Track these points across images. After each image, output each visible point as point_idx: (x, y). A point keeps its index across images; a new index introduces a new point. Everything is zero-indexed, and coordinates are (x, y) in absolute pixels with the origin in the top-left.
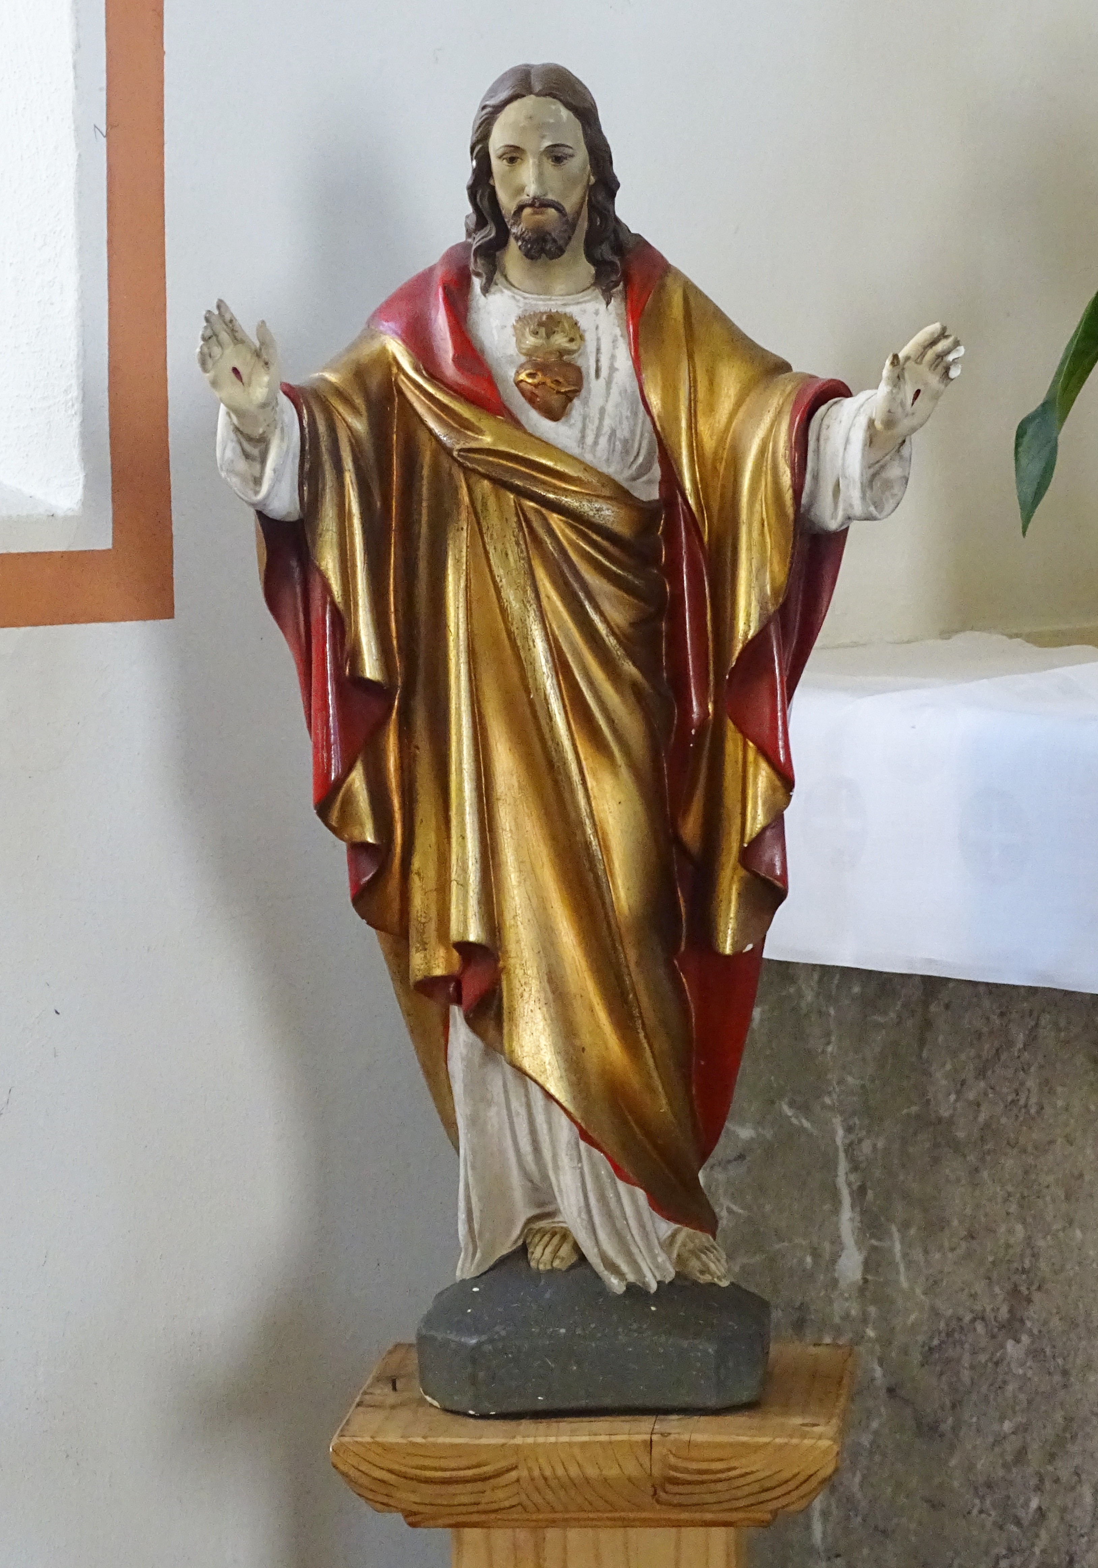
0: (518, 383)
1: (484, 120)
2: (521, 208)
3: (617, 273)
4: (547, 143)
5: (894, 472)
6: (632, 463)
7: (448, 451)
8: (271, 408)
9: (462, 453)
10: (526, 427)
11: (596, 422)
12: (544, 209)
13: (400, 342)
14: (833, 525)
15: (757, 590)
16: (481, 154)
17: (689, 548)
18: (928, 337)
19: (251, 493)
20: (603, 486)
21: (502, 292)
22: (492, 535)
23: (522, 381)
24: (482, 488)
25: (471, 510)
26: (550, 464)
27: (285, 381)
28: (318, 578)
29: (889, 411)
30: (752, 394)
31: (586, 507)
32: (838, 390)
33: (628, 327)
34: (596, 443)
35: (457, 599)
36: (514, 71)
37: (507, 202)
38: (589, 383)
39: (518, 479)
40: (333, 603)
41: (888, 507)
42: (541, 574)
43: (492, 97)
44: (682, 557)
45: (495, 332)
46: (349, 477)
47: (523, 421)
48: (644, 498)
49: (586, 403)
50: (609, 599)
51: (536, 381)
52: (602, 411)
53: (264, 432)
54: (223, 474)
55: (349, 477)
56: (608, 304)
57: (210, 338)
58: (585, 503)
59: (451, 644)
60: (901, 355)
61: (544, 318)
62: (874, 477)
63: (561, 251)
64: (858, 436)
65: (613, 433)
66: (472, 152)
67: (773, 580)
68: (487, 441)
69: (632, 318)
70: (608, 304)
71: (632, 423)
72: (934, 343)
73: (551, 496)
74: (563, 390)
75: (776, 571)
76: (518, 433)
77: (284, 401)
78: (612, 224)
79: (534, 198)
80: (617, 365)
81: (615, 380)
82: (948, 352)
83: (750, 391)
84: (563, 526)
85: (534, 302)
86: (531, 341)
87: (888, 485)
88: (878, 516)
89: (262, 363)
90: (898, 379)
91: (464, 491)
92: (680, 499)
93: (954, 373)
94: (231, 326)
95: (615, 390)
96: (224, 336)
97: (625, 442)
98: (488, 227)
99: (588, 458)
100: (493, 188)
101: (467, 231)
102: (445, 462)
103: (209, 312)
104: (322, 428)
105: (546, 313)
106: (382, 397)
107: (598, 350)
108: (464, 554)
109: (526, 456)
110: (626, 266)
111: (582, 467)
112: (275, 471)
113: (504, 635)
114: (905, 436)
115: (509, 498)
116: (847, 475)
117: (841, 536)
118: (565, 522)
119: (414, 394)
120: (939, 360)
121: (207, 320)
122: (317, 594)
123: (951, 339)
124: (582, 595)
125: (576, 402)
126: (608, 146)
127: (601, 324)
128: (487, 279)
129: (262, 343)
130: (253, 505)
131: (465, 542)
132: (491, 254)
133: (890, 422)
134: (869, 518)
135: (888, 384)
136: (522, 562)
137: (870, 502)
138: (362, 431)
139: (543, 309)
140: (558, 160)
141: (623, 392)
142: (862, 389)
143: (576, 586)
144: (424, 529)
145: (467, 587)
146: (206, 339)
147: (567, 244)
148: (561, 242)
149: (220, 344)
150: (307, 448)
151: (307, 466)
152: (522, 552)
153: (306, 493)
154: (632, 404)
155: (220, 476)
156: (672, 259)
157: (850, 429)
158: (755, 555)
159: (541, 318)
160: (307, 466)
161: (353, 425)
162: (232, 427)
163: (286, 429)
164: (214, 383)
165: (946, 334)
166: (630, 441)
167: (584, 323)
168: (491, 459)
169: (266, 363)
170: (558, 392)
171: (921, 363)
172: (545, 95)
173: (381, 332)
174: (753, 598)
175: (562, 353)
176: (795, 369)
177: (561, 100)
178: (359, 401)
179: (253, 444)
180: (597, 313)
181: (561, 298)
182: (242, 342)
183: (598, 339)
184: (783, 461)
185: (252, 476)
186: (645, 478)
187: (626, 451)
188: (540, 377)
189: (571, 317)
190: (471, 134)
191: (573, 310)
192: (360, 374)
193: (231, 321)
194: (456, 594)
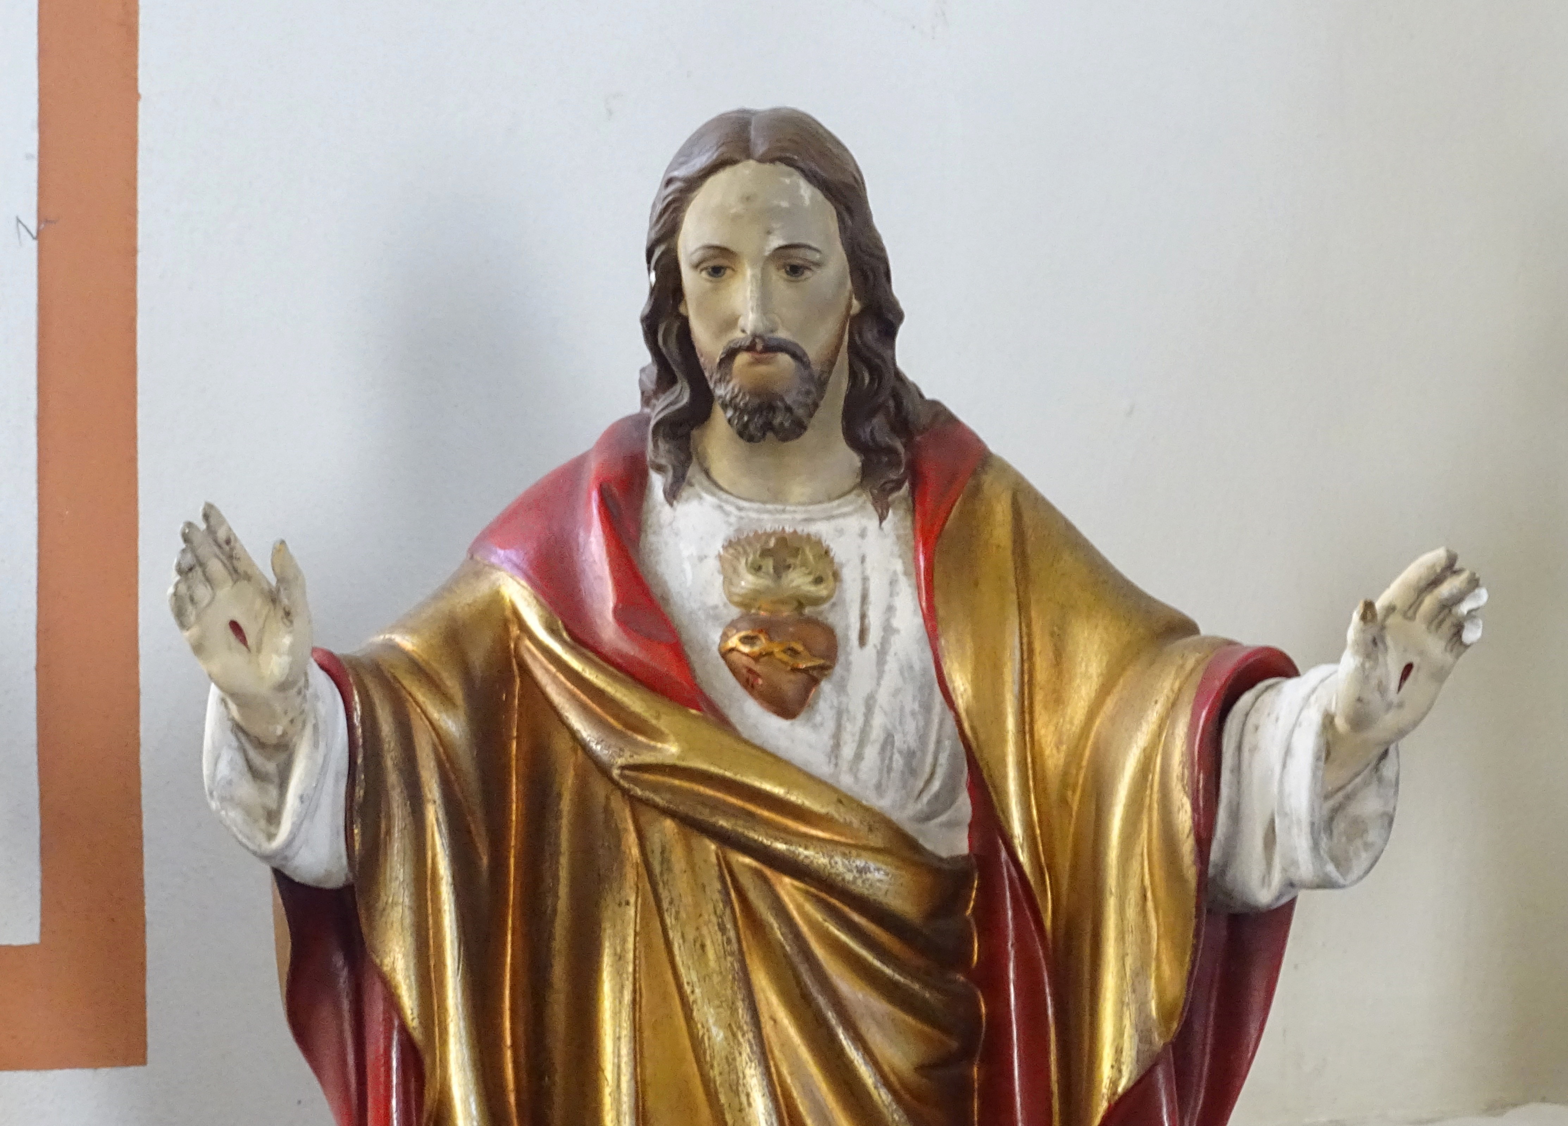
0: (726, 654)
1: (668, 205)
2: (731, 354)
3: (898, 465)
4: (776, 242)
5: (1369, 804)
6: (921, 792)
7: (603, 770)
8: (295, 690)
9: (627, 772)
10: (739, 728)
11: (860, 720)
12: (771, 355)
13: (523, 583)
14: (1264, 895)
15: (1133, 1008)
16: (663, 262)
17: (1019, 938)
18: (1423, 571)
19: (261, 838)
20: (871, 830)
21: (701, 498)
22: (677, 913)
23: (732, 650)
24: (662, 831)
25: (642, 870)
26: (778, 791)
27: (318, 644)
28: (378, 988)
29: (1359, 700)
30: (1129, 673)
31: (840, 866)
32: (1271, 666)
33: (916, 559)
34: (859, 756)
35: (617, 1025)
36: (722, 120)
37: (708, 343)
38: (848, 654)
39: (723, 818)
40: (404, 1029)
41: (1357, 869)
42: (762, 981)
43: (682, 164)
44: (1007, 953)
45: (687, 567)
46: (434, 814)
47: (734, 717)
48: (944, 853)
49: (841, 688)
50: (879, 1024)
51: (756, 649)
52: (870, 703)
53: (285, 734)
54: (214, 805)
55: (434, 814)
56: (882, 518)
57: (191, 569)
58: (838, 859)
59: (608, 1101)
60: (1380, 604)
61: (772, 543)
62: (1335, 815)
63: (799, 428)
64: (1306, 744)
65: (888, 741)
66: (649, 261)
67: (1161, 991)
68: (670, 750)
69: (924, 545)
70: (882, 518)
71: (921, 723)
72: (1435, 582)
73: (781, 846)
74: (803, 666)
75: (1167, 977)
76: (727, 740)
77: (321, 682)
78: (890, 382)
79: (755, 336)
80: (896, 623)
81: (892, 651)
82: (1458, 599)
83: (1124, 669)
84: (801, 899)
85: (753, 515)
86: (748, 581)
87: (1358, 827)
88: (1341, 881)
89: (281, 613)
90: (1373, 645)
91: (631, 838)
92: (1004, 855)
93: (1471, 634)
94: (228, 549)
95: (892, 665)
96: (216, 567)
97: (910, 755)
98: (677, 388)
99: (846, 781)
100: (685, 320)
101: (643, 393)
102: (600, 789)
103: (189, 525)
104: (387, 727)
105: (774, 533)
106: (495, 681)
107: (864, 598)
108: (630, 945)
109: (738, 778)
110: (913, 454)
111: (835, 797)
112: (302, 798)
113: (697, 1082)
114: (1388, 743)
115: (706, 849)
116: (1287, 810)
117: (1278, 918)
118: (807, 893)
119: (547, 671)
120: (1446, 611)
121: (186, 538)
122: (376, 1011)
123: (1464, 576)
124: (831, 1016)
125: (826, 686)
126: (882, 249)
127: (870, 554)
128: (674, 476)
129: (281, 580)
130: (266, 858)
131: (632, 925)
132: (682, 432)
133: (1360, 720)
134: (1326, 884)
135: (1356, 652)
136: (729, 959)
137: (1326, 857)
138: (457, 735)
139: (769, 528)
140: (795, 271)
141: (906, 669)
142: (1315, 663)
143: (821, 1001)
144: (563, 903)
145: (635, 1003)
146: (184, 572)
147: (811, 415)
148: (800, 412)
149: (208, 580)
150: (360, 761)
151: (360, 793)
152: (729, 941)
153: (357, 838)
154: (921, 688)
155: (208, 806)
156: (996, 442)
157: (1292, 732)
158: (1132, 949)
159: (767, 542)
160: (360, 793)
161: (442, 724)
162: (229, 724)
163: (321, 727)
164: (198, 648)
165: (1457, 566)
166: (919, 754)
167: (842, 550)
168: (677, 782)
169: (288, 614)
170: (795, 670)
171: (1412, 618)
172: (772, 161)
173: (492, 566)
174: (1127, 1022)
175: (801, 602)
176: (1204, 631)
177: (798, 168)
178: (453, 685)
179: (266, 753)
180: (863, 534)
181: (800, 508)
182: (248, 578)
183: (865, 579)
184: (1179, 787)
185: (264, 807)
186: (943, 818)
187: (911, 770)
188: (762, 644)
189: (819, 543)
190: (647, 225)
191: (822, 529)
192: (453, 637)
193: (228, 542)
194: (616, 1014)
